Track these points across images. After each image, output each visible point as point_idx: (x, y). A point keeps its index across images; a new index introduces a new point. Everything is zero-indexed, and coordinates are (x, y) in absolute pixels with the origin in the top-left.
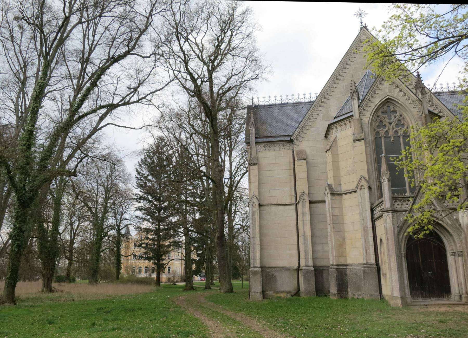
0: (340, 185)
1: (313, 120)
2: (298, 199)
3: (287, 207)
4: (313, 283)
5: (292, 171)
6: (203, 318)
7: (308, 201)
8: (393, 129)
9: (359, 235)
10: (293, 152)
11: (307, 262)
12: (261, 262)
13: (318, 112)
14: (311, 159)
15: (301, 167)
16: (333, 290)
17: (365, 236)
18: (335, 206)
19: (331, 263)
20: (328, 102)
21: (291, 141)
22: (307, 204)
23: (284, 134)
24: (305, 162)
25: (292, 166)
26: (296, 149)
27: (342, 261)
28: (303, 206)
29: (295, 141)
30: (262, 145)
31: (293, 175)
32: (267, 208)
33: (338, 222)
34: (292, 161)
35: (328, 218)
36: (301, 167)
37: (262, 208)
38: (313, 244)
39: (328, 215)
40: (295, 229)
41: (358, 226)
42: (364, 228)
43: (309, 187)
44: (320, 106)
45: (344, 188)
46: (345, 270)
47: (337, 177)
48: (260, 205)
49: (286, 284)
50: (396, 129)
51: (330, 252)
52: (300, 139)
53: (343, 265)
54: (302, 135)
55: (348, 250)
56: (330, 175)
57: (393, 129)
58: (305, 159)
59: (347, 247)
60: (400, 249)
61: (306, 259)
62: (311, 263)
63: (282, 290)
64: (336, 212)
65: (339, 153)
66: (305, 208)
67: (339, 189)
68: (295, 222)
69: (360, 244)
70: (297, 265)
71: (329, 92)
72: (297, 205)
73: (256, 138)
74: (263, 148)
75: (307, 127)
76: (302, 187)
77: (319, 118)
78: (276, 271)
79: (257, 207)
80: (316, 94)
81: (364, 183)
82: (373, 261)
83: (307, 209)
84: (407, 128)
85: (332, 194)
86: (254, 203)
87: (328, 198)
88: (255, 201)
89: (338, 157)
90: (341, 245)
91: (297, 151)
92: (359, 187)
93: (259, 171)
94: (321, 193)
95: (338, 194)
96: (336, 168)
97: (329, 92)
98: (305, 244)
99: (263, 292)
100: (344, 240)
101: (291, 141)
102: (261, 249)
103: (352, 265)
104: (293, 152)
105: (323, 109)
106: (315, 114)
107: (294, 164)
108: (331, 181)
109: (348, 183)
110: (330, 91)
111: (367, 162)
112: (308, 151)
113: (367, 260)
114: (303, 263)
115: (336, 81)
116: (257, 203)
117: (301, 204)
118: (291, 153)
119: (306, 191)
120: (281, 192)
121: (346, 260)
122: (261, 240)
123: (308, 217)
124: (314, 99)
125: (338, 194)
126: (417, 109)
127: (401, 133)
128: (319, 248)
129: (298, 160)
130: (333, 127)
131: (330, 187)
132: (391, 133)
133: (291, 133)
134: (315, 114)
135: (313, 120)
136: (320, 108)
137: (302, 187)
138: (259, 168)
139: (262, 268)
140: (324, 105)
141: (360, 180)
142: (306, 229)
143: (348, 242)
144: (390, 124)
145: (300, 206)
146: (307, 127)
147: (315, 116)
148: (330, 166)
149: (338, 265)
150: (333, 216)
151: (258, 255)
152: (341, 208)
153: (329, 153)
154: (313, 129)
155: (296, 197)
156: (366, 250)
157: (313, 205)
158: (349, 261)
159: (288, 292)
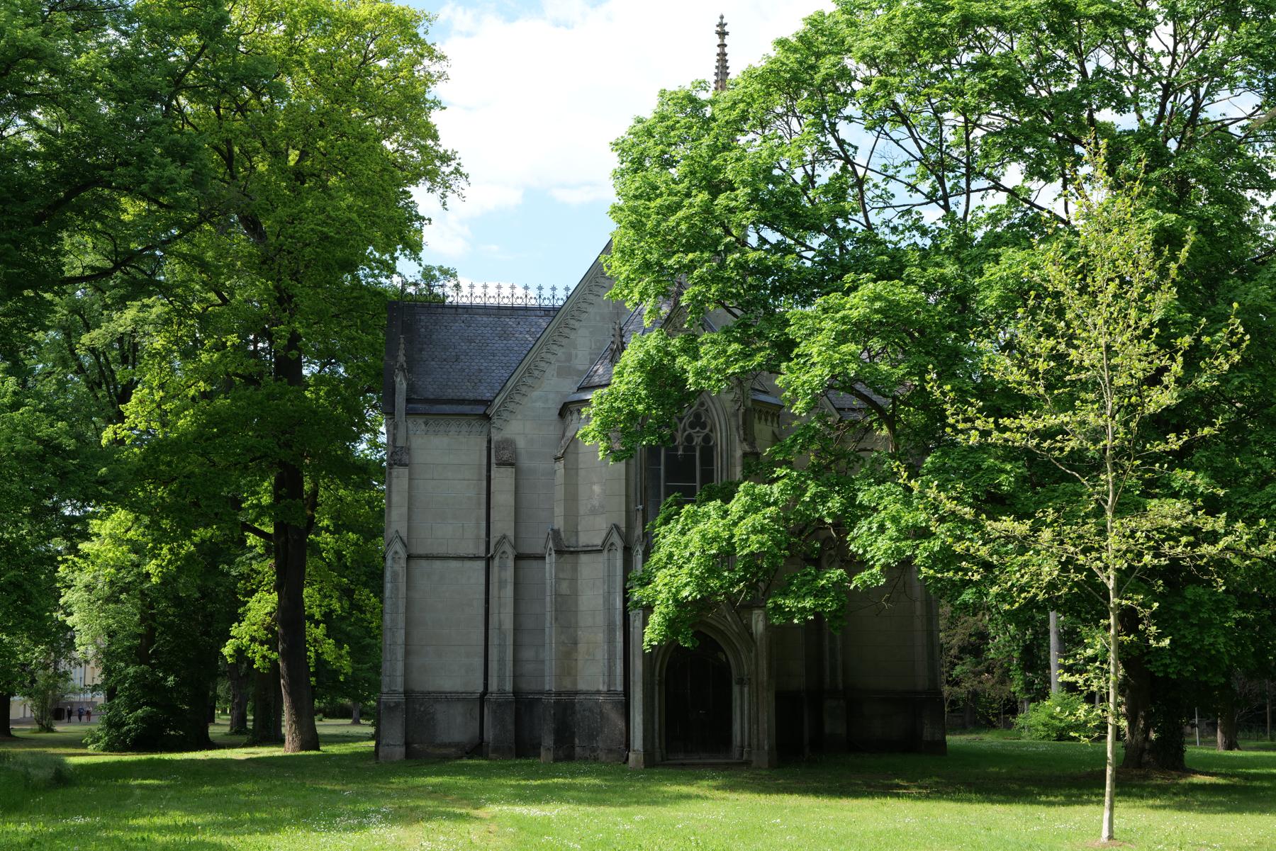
0: (577, 533)
1: (536, 373)
2: (492, 551)
3: (468, 564)
4: (511, 727)
5: (484, 483)
6: (781, 601)
7: (511, 557)
8: (685, 430)
9: (601, 637)
10: (489, 442)
11: (501, 683)
12: (406, 682)
13: (549, 356)
14: (525, 462)
15: (503, 479)
16: (548, 741)
17: (611, 641)
18: (561, 576)
19: (547, 688)
20: (572, 336)
21: (486, 417)
22: (510, 563)
23: (471, 396)
24: (511, 470)
25: (484, 472)
26: (496, 436)
27: (567, 685)
28: (502, 567)
29: (495, 419)
30: (421, 421)
31: (485, 492)
32: (424, 563)
33: (566, 607)
34: (485, 461)
35: (548, 599)
36: (503, 479)
37: (413, 563)
38: (517, 646)
39: (548, 593)
40: (482, 611)
41: (600, 619)
42: (609, 625)
43: (516, 522)
44: (555, 342)
45: (584, 539)
46: (573, 704)
47: (572, 515)
48: (410, 557)
49: (455, 726)
50: (689, 431)
51: (547, 663)
52: (505, 415)
53: (569, 693)
54: (511, 406)
55: (580, 663)
56: (559, 510)
57: (685, 430)
58: (512, 465)
59: (580, 658)
60: (653, 675)
61: (501, 678)
62: (509, 687)
63: (447, 740)
64: (564, 588)
65: (581, 466)
66: (504, 571)
67: (573, 541)
68: (483, 596)
69: (601, 654)
70: (481, 689)
71: (576, 313)
72: (488, 560)
73: (409, 401)
74: (423, 426)
75: (524, 389)
76: (503, 525)
77: (551, 371)
78: (436, 700)
79: (403, 563)
80: (567, 289)
81: (616, 539)
82: (620, 688)
83: (509, 574)
84: (711, 431)
85: (559, 552)
86: (396, 553)
87: (551, 559)
88: (398, 549)
89: (577, 474)
90: (569, 649)
91: (497, 442)
92: (606, 546)
93: (410, 479)
94: (536, 542)
95: (572, 553)
96: (572, 498)
97: (576, 313)
98: (502, 646)
99: (407, 744)
100: (576, 643)
101: (486, 417)
102: (407, 653)
103: (586, 693)
104: (489, 442)
105: (560, 351)
106: (542, 359)
107: (489, 470)
108: (559, 523)
109: (593, 530)
110: (579, 309)
111: (627, 496)
112: (521, 443)
113: (609, 686)
114: (494, 686)
115: (595, 289)
116: (403, 554)
117: (497, 561)
118: (485, 444)
119: (511, 534)
120: (454, 530)
121: (575, 683)
122: (407, 634)
123: (509, 591)
124: (561, 303)
125: (572, 553)
126: (731, 396)
127: (698, 440)
128: (527, 654)
129: (500, 464)
130: (573, 407)
131: (556, 533)
132: (680, 439)
133: (488, 396)
134: (542, 359)
135: (536, 373)
136: (555, 347)
137: (503, 525)
138: (410, 474)
139: (408, 693)
140: (564, 342)
141: (609, 534)
142: (504, 616)
143: (582, 647)
144: (681, 420)
145: (496, 563)
146: (524, 389)
147: (543, 364)
148: (559, 493)
149: (558, 694)
150: (558, 595)
151: (400, 666)
152: (574, 581)
153: (560, 465)
154: (535, 394)
155: (488, 543)
156: (610, 667)
157: (524, 563)
158: (582, 686)
159: (456, 745)
